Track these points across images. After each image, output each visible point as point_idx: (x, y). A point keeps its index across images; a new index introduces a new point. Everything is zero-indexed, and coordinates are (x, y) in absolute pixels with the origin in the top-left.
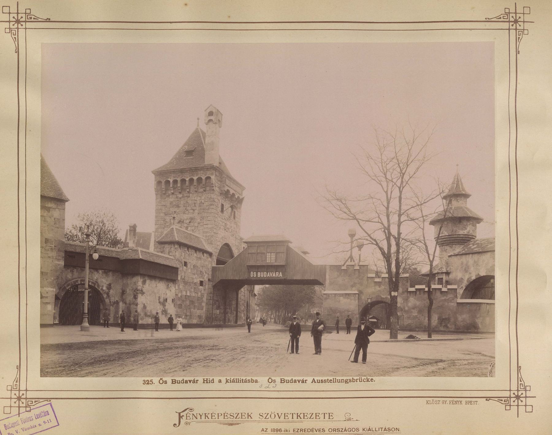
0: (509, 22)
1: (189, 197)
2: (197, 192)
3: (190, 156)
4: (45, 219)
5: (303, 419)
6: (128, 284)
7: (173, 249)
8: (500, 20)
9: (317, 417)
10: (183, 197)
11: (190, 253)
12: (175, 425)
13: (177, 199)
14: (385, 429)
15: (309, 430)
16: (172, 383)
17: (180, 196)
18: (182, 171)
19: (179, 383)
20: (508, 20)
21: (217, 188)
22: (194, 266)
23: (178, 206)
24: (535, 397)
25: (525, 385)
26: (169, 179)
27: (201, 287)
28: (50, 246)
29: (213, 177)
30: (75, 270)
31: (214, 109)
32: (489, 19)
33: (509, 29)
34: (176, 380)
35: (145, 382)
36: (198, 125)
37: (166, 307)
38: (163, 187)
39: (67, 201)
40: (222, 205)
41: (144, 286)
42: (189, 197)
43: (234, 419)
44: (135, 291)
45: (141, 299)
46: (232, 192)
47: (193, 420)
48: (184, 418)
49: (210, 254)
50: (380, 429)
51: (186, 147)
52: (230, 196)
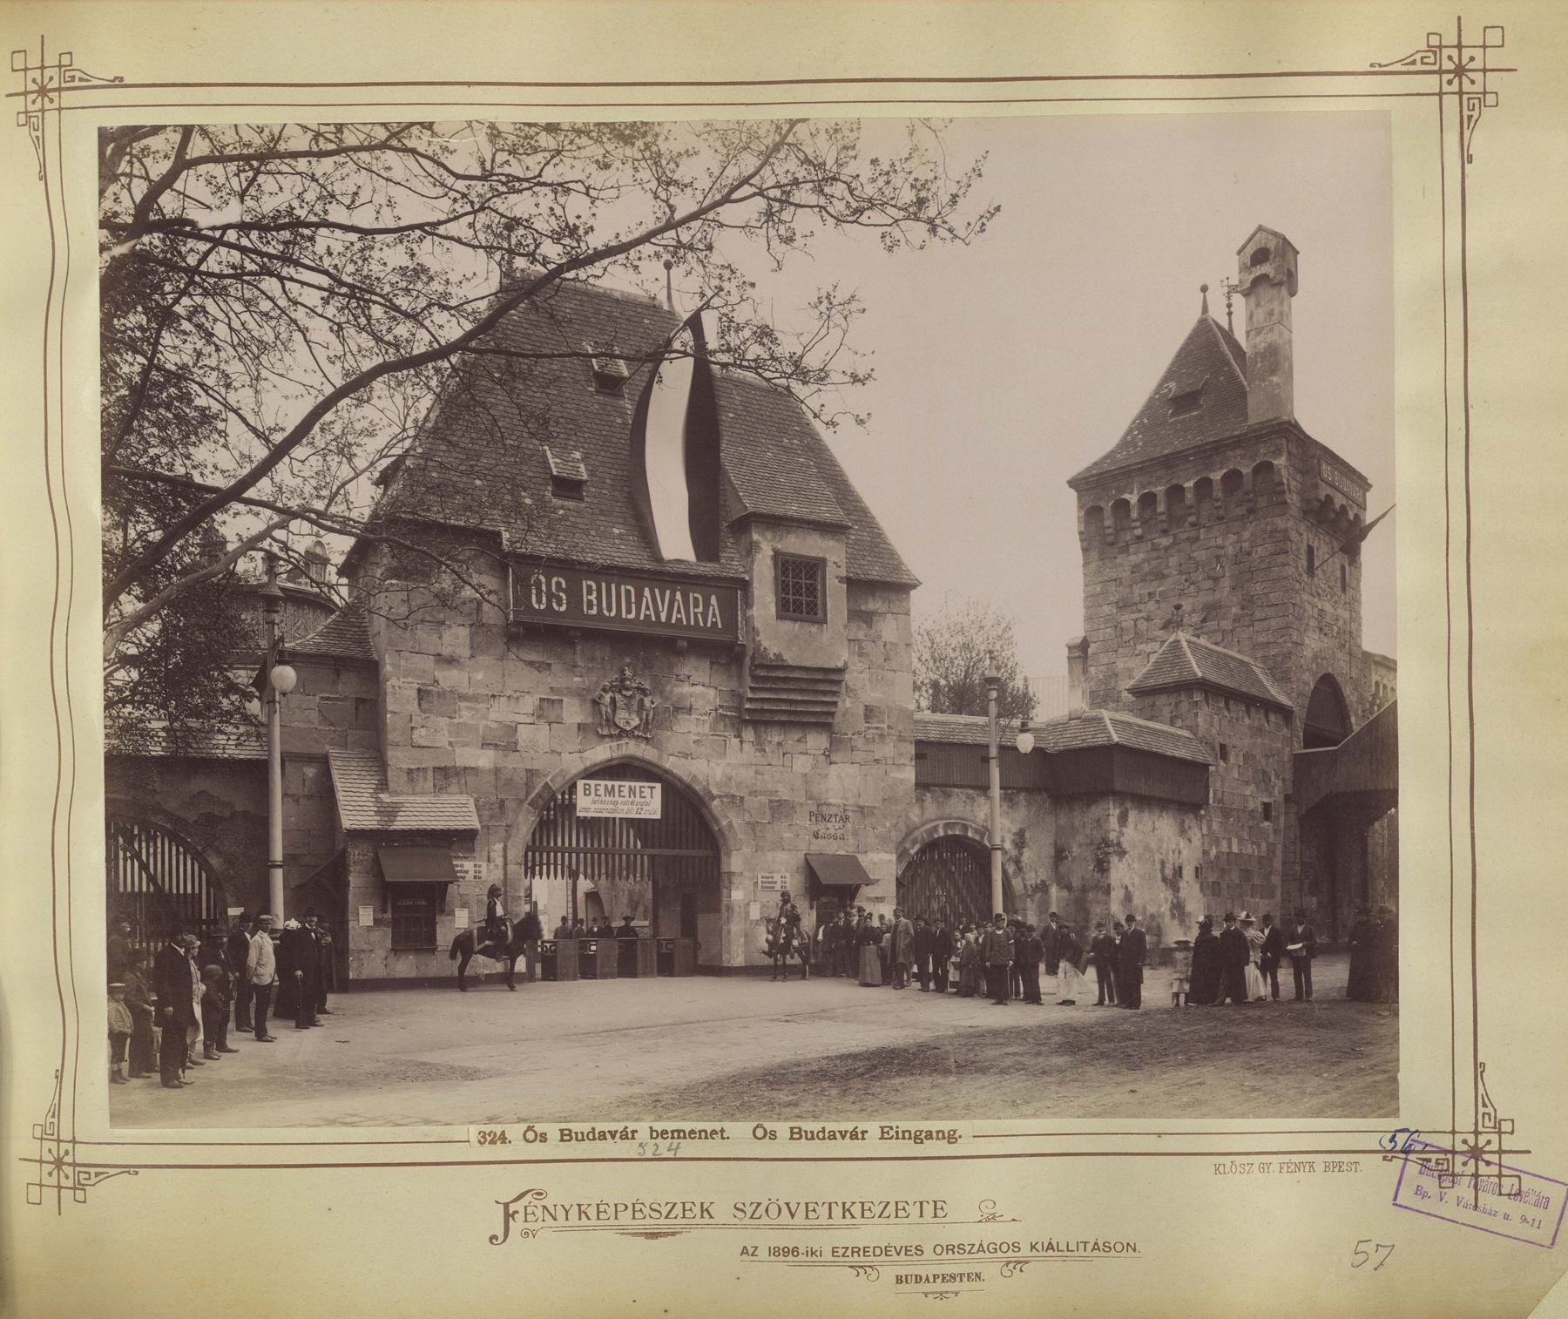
0: (1440, 72)
1: (1197, 539)
2: (1223, 518)
3: (1189, 411)
4: (861, 648)
5: (859, 1220)
6: (1072, 827)
7: (1185, 706)
8: (1412, 68)
9: (901, 1213)
10: (1174, 544)
11: (1234, 715)
12: (493, 1238)
13: (1155, 554)
14: (1096, 1247)
15: (878, 1251)
16: (562, 1140)
17: (1165, 541)
18: (1170, 462)
19: (583, 1140)
20: (1436, 68)
21: (1295, 496)
22: (1247, 757)
23: (1160, 576)
24: (1529, 1152)
25: (1499, 1117)
26: (1127, 496)
27: (1266, 824)
28: (877, 728)
29: (1280, 462)
30: (928, 795)
31: (1270, 237)
32: (1380, 66)
33: (1440, 94)
34: (804, 1129)
35: (484, 1137)
36: (1205, 309)
37: (1182, 894)
38: (1108, 523)
39: (915, 587)
40: (1310, 550)
41: (1124, 830)
42: (1197, 539)
43: (663, 1221)
44: (1099, 848)
45: (1120, 873)
46: (1339, 501)
47: (544, 1224)
48: (520, 1217)
49: (1286, 713)
50: (1081, 1246)
51: (1172, 385)
52: (1332, 515)
